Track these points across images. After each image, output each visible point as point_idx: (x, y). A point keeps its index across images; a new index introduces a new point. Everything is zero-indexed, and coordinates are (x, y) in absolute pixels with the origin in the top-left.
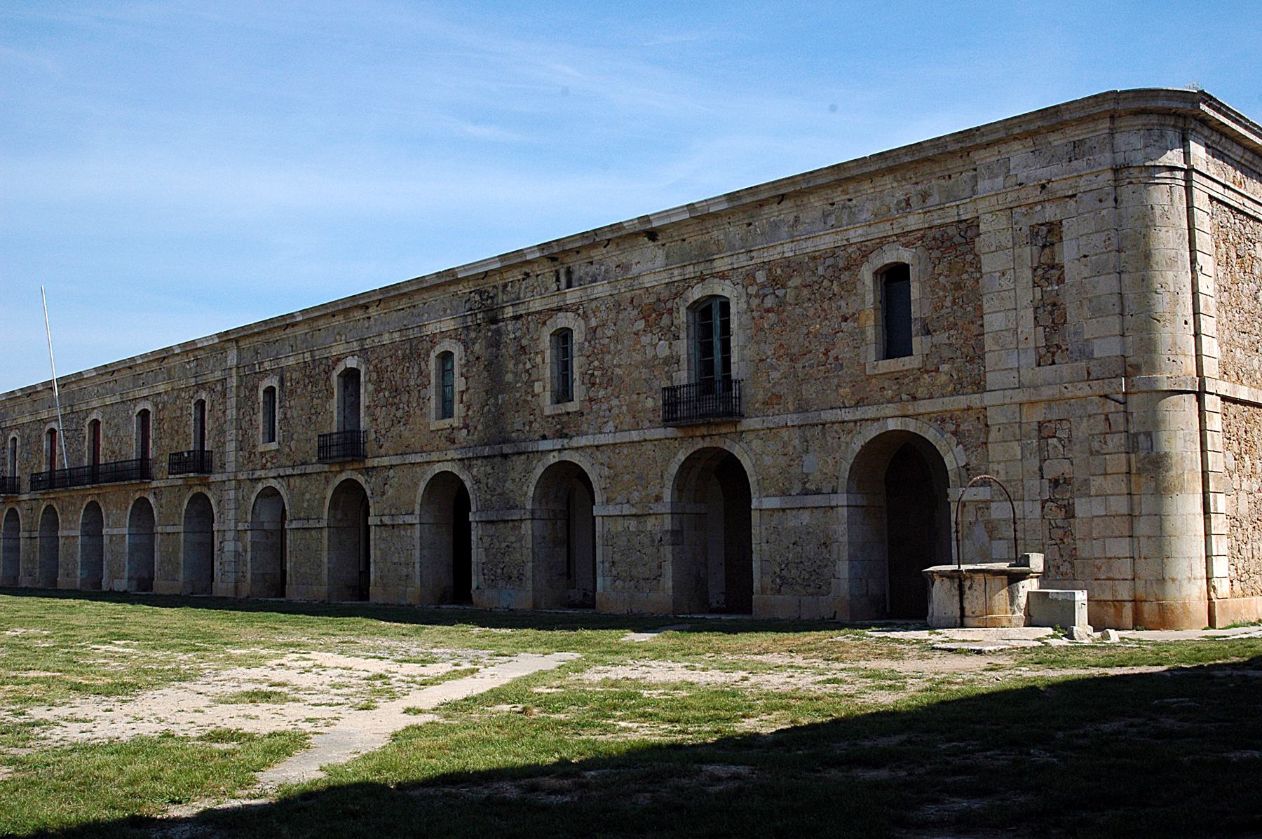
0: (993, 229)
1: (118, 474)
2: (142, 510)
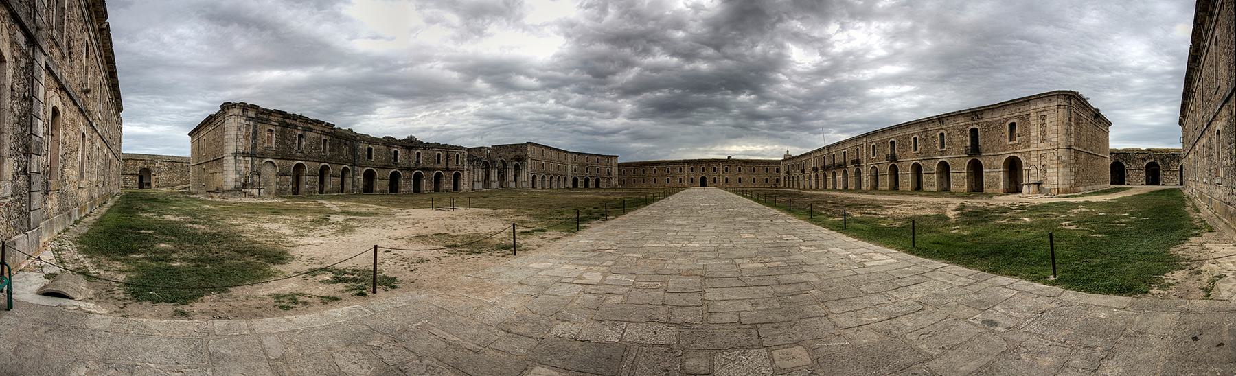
0: (1033, 116)
1: (840, 166)
2: (845, 172)
